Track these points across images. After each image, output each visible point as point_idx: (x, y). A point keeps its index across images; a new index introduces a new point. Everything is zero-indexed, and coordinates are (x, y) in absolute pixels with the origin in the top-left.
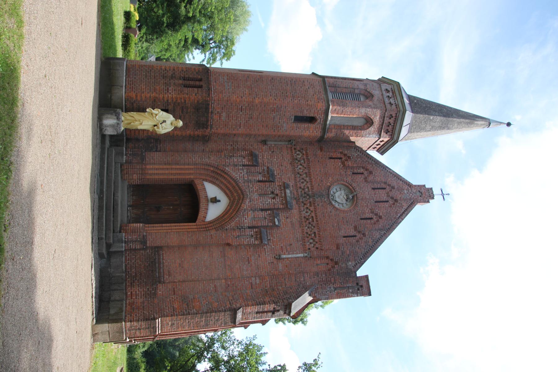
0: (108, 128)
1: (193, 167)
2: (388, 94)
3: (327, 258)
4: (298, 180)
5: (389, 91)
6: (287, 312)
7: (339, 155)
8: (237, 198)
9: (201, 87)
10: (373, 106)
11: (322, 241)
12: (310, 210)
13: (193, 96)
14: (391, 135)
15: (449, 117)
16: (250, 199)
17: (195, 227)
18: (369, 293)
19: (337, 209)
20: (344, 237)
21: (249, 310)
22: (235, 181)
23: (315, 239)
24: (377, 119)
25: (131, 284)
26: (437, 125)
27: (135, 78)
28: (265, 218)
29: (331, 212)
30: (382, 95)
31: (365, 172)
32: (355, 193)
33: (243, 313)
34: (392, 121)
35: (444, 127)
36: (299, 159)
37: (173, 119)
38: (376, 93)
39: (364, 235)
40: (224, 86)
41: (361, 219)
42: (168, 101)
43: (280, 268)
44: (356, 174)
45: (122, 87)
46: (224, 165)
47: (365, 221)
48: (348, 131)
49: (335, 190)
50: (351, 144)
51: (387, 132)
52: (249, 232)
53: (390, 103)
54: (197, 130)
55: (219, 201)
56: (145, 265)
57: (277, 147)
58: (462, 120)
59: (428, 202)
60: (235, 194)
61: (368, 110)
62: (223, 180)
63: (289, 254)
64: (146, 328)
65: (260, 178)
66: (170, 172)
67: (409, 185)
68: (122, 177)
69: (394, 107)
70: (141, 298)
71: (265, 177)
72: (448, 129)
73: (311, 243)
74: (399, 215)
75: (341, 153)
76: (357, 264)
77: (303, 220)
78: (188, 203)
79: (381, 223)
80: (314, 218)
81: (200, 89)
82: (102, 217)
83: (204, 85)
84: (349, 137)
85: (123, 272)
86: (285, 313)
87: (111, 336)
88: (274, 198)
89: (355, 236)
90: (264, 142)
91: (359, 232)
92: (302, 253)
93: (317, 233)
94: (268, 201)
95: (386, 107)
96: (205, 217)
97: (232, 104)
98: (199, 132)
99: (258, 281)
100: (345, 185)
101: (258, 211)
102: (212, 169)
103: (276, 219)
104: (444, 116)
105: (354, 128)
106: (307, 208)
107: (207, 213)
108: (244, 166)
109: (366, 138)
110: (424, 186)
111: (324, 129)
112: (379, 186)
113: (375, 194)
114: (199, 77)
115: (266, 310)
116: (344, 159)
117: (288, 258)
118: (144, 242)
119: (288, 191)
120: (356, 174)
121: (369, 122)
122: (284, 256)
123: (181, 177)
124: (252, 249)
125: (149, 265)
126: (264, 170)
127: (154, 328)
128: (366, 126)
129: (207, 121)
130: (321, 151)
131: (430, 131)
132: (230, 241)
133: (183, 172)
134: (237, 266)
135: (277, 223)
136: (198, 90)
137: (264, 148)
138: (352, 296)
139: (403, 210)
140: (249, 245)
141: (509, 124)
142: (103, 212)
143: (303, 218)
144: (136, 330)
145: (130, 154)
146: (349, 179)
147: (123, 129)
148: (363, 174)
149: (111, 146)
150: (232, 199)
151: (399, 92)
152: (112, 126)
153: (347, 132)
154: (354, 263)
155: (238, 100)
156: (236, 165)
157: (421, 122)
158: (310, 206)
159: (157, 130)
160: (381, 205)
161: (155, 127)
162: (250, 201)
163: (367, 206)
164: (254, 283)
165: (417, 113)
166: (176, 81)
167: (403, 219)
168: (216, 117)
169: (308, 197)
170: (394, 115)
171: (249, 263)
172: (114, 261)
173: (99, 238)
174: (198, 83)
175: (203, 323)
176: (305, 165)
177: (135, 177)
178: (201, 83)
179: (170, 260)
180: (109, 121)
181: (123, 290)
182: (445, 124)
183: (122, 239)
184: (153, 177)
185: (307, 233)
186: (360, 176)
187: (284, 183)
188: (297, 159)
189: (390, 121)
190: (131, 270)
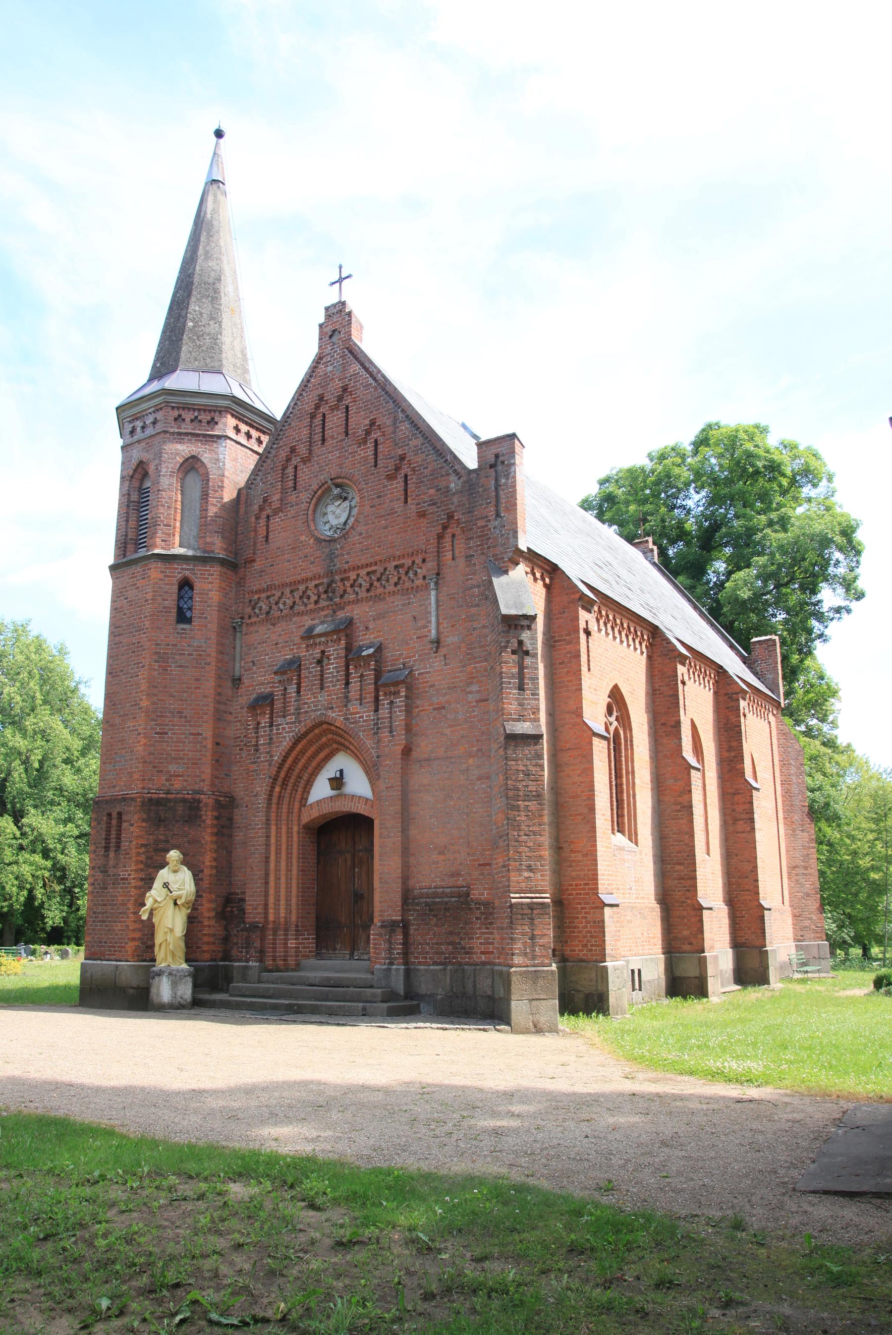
0: (179, 993)
2: (139, 429)
3: (440, 537)
4: (302, 608)
5: (133, 427)
6: (525, 623)
7: (262, 522)
8: (330, 736)
9: (120, 814)
10: (157, 462)
11: (410, 550)
12: (355, 581)
13: (135, 830)
14: (220, 412)
15: (192, 283)
16: (328, 709)
20: (406, 502)
21: (512, 707)
23: (406, 567)
24: (184, 449)
25: (467, 953)
26: (207, 309)
27: (106, 942)
28: (362, 676)
29: (361, 534)
30: (139, 442)
33: (518, 720)
34: (188, 416)
35: (213, 293)
37: (166, 868)
38: (137, 454)
39: (402, 458)
40: (121, 769)
41: (376, 466)
42: (142, 879)
45: (117, 966)
46: (270, 765)
47: (380, 456)
48: (210, 507)
49: (327, 526)
50: (243, 498)
51: (212, 422)
52: (384, 712)
54: (204, 821)
56: (436, 925)
57: (246, 654)
58: (201, 252)
59: (349, 314)
60: (324, 739)
61: (164, 470)
64: (532, 924)
67: (319, 360)
68: (293, 970)
69: (159, 415)
70: (492, 933)
72: (219, 280)
74: (371, 381)
75: (258, 518)
76: (455, 471)
78: (342, 834)
79: (385, 420)
80: (369, 569)
81: (124, 817)
82: (330, 1007)
83: (118, 809)
84: (224, 506)
85: (445, 969)
86: (529, 628)
87: (542, 997)
90: (237, 681)
91: (397, 469)
93: (396, 563)
95: (159, 433)
96: (367, 799)
97: (150, 754)
98: (208, 816)
100: (316, 505)
101: (348, 692)
102: (277, 789)
104: (189, 295)
105: (205, 496)
106: (352, 586)
107: (360, 797)
108: (271, 725)
109: (228, 466)
111: (203, 560)
112: (318, 430)
113: (332, 437)
114: (105, 818)
115: (515, 670)
116: (269, 511)
117: (438, 623)
119: (319, 630)
121: (191, 465)
122: (433, 632)
123: (295, 851)
124: (419, 702)
125: (435, 916)
126: (280, 681)
128: (201, 470)
129: (184, 800)
131: (220, 323)
132: (399, 749)
133: (284, 847)
134: (448, 731)
135: (371, 651)
136: (126, 821)
137: (246, 681)
138: (514, 477)
140: (409, 710)
141: (219, 134)
142: (321, 1005)
143: (369, 595)
144: (533, 945)
145: (247, 952)
146: (304, 496)
147: (185, 966)
148: (296, 467)
149: (227, 991)
150: (335, 746)
151: (133, 407)
152: (174, 985)
153: (212, 511)
154: (453, 477)
155: (143, 741)
156: (271, 739)
157: (200, 347)
158: (348, 579)
159: (183, 900)
161: (179, 903)
162: (332, 708)
164: (478, 696)
165: (179, 358)
166: (111, 863)
167: (379, 371)
168: (177, 784)
169: (334, 585)
170: (176, 413)
171: (443, 708)
172: (423, 988)
173: (364, 1015)
175: (533, 805)
178: (115, 815)
179: (430, 876)
180: (164, 991)
181: (475, 970)
182: (207, 290)
183: (384, 970)
185: (396, 584)
189: (188, 420)
190: (443, 953)
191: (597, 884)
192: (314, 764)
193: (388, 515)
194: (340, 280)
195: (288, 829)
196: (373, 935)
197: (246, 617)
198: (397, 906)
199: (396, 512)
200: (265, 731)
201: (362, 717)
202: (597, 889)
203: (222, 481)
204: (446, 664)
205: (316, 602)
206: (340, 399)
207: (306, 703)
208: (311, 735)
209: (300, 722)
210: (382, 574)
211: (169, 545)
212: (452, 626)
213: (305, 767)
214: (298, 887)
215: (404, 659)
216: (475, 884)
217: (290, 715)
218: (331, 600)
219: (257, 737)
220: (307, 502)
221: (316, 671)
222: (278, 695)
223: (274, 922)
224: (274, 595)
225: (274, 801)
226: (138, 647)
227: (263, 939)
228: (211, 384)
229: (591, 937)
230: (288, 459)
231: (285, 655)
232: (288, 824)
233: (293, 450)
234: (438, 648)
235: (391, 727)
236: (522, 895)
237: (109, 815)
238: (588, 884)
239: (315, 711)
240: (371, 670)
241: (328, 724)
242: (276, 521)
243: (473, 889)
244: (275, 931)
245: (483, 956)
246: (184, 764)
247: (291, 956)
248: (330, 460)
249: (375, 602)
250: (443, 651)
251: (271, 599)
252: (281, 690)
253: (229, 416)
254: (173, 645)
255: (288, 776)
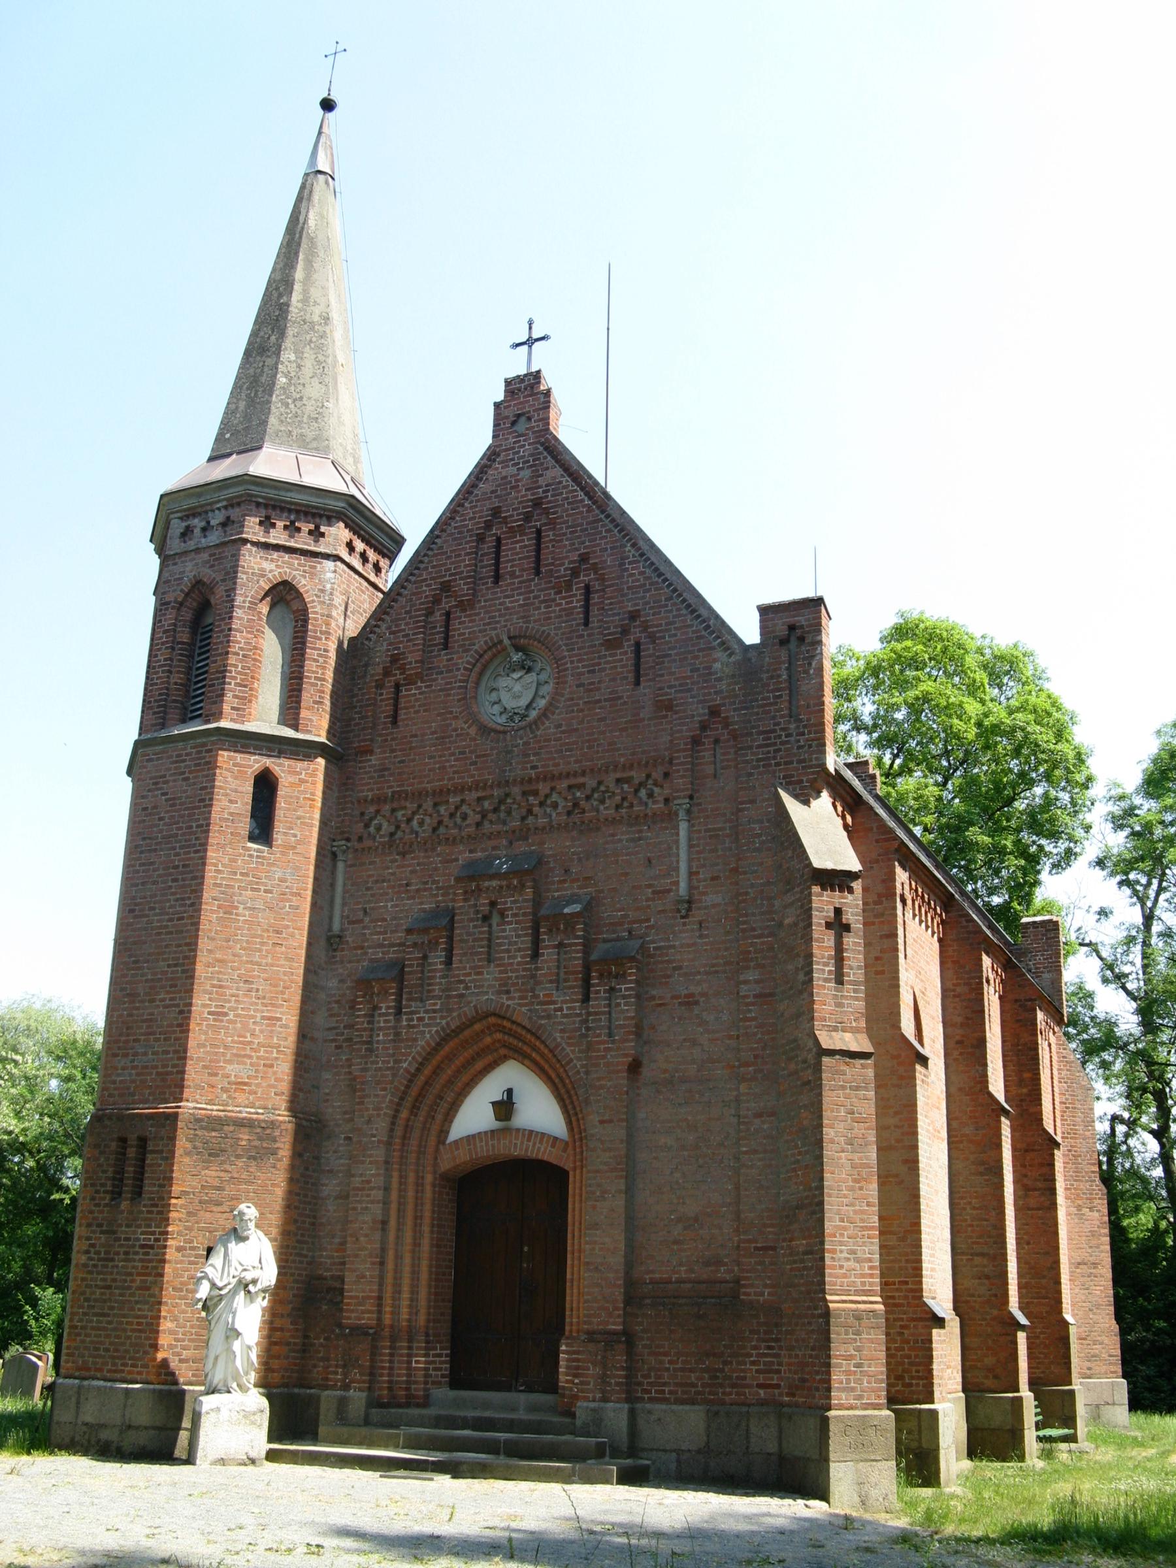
1: (395, 1174)
5: (188, 527)
7: (387, 693)
12: (547, 796)
17: (578, 1172)
18: (815, 604)
19: (550, 704)
22: (444, 1039)
23: (637, 782)
28: (561, 945)
30: (197, 550)
31: (445, 605)
32: (506, 642)
36: (392, 829)
38: (189, 570)
39: (634, 616)
41: (586, 623)
43: (718, 899)
44: (447, 638)
46: (394, 1075)
47: (594, 611)
49: (496, 709)
52: (598, 1003)
53: (224, 525)
55: (510, 1092)
59: (548, 393)
60: (488, 1040)
62: (443, 1078)
63: (677, 869)
65: (437, 959)
66: (408, 1248)
67: (491, 456)
71: (437, 943)
73: (651, 795)
74: (581, 495)
75: (380, 685)
77: (576, 818)
80: (573, 781)
88: (502, 914)
89: (638, 645)
91: (625, 631)
92: (677, 827)
93: (618, 775)
94: (512, 933)
96: (556, 1139)
99: (751, 975)
100: (481, 674)
102: (404, 1114)
103: (566, 911)
108: (399, 1012)
110: (497, 405)
112: (489, 561)
113: (513, 575)
114: (114, 1145)
117: (691, 874)
118: (608, 1339)
120: (447, 638)
121: (284, 596)
122: (683, 885)
123: (427, 1214)
126: (415, 945)
127: (858, 1316)
130: (371, 752)
135: (577, 908)
139: (567, 481)
141: (328, 105)
145: (345, 1375)
146: (464, 660)
150: (503, 1051)
154: (719, 654)
156: (397, 1034)
158: (535, 793)
160: (547, 557)
163: (548, 602)
164: (758, 989)
171: (697, 1003)
174: (132, 1152)
176: (411, 806)
177: (419, 1362)
184: (423, 1303)
185: (618, 807)
186: (455, 624)
187: (458, 879)
188: (392, 835)
190: (694, 1385)
191: (921, 1283)
192: (465, 1078)
193: (606, 700)
194: (530, 342)
195: (418, 1177)
196: (565, 1352)
197: (354, 838)
198: (616, 1309)
199: (620, 698)
200: (386, 1021)
201: (561, 1009)
202: (921, 1290)
203: (328, 624)
204: (701, 936)
205: (478, 825)
206: (528, 517)
207: (461, 982)
208: (467, 1033)
209: (450, 1011)
210: (594, 790)
211: (244, 716)
212: (713, 879)
213: (450, 1082)
214: (430, 1273)
215: (629, 923)
216: (747, 1278)
217: (433, 997)
218: (504, 823)
219: (372, 1030)
220: (465, 669)
221: (481, 933)
222: (411, 966)
223: (392, 1326)
224: (405, 808)
225: (399, 1132)
226: (183, 873)
227: (374, 1352)
228: (319, 475)
229: (911, 1364)
230: (437, 600)
231: (422, 903)
232: (417, 1172)
233: (446, 587)
234: (689, 909)
235: (609, 1028)
236: (844, 1298)
237: (123, 1140)
238: (906, 1283)
239: (477, 994)
240: (578, 937)
241: (499, 1016)
242: (411, 693)
243: (744, 1286)
244: (393, 1339)
245: (762, 1392)
246: (251, 1064)
247: (416, 1382)
248: (507, 609)
249: (581, 832)
250: (697, 915)
251: (400, 814)
252: (417, 959)
253: (342, 525)
254: (242, 874)
255: (421, 1095)
